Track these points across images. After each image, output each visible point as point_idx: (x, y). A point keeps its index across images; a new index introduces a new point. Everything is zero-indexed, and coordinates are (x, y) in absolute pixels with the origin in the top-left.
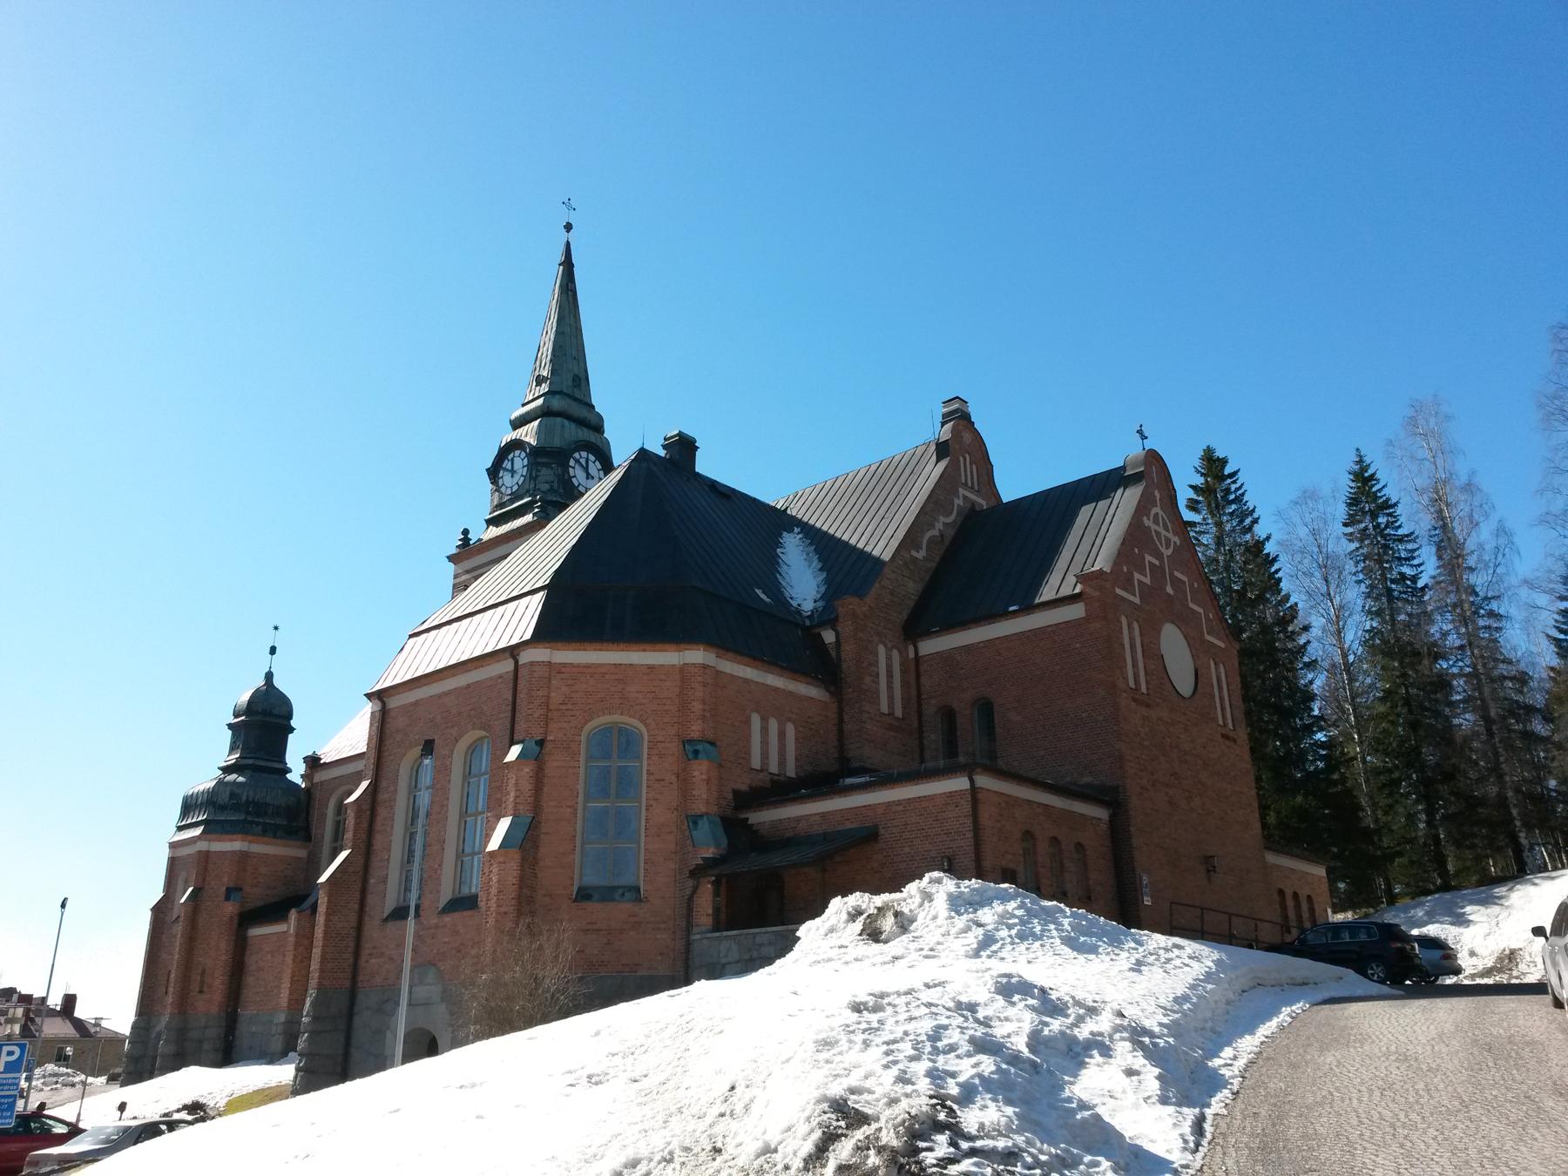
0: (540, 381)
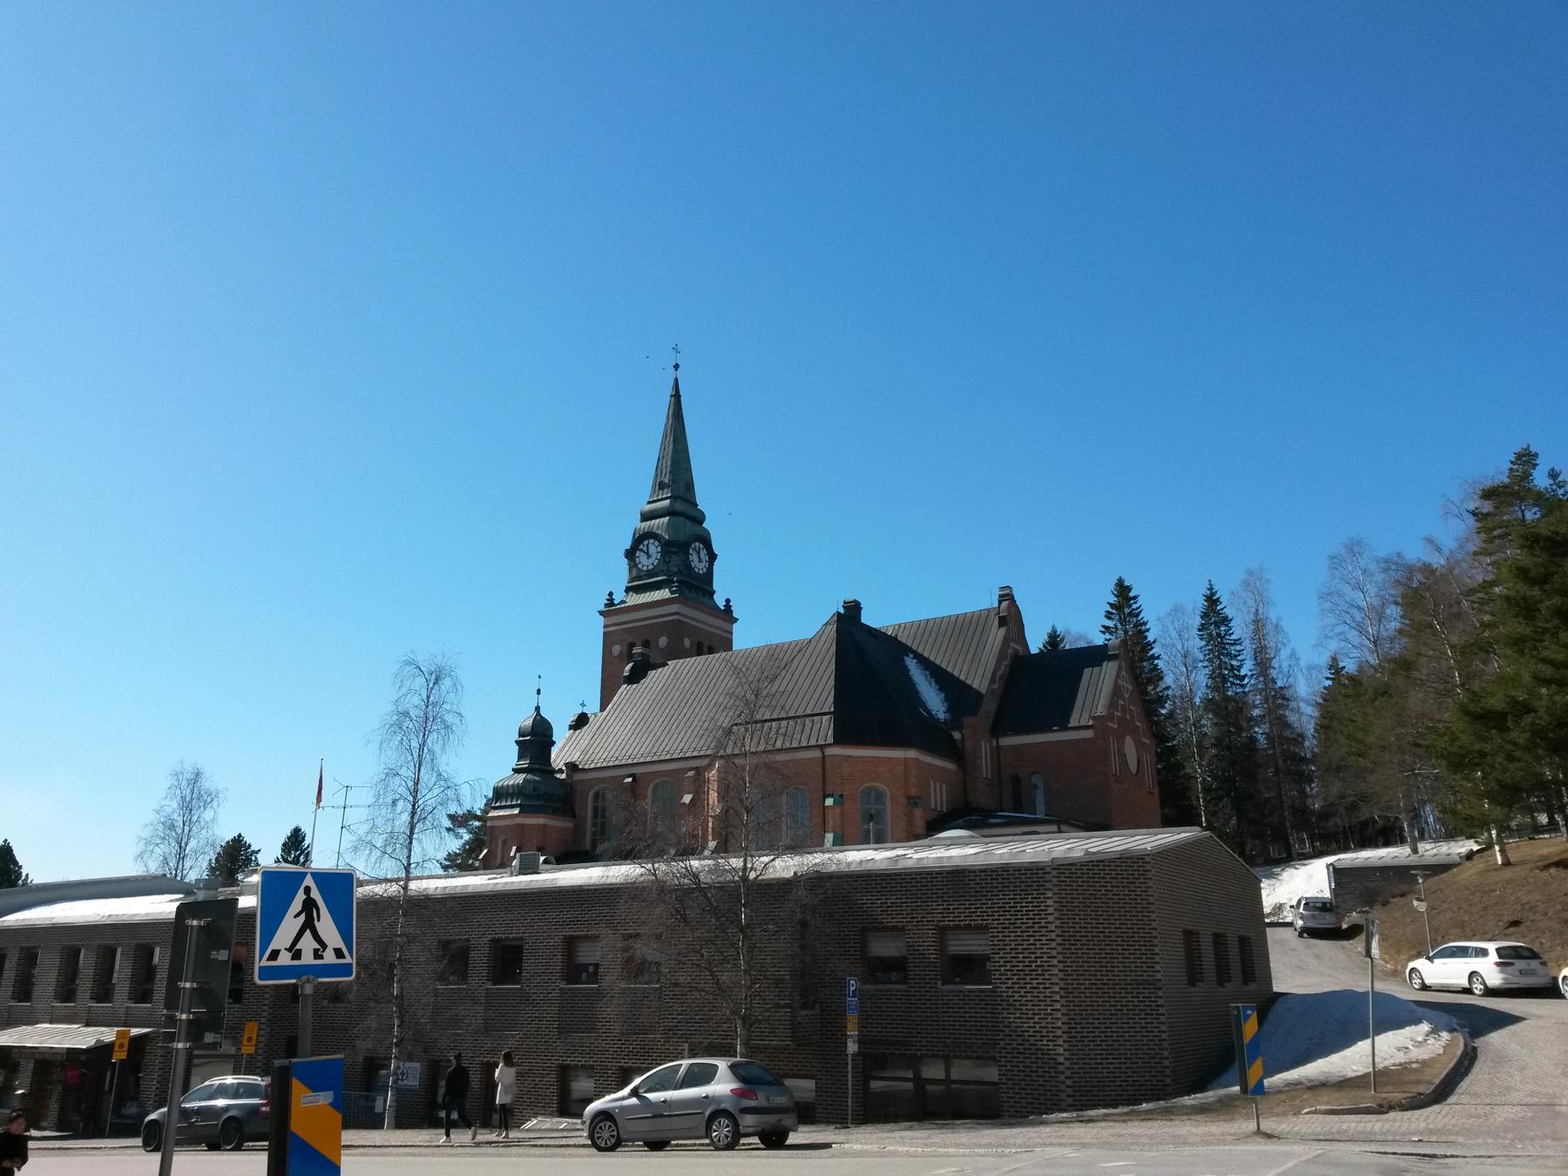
0: (662, 486)
